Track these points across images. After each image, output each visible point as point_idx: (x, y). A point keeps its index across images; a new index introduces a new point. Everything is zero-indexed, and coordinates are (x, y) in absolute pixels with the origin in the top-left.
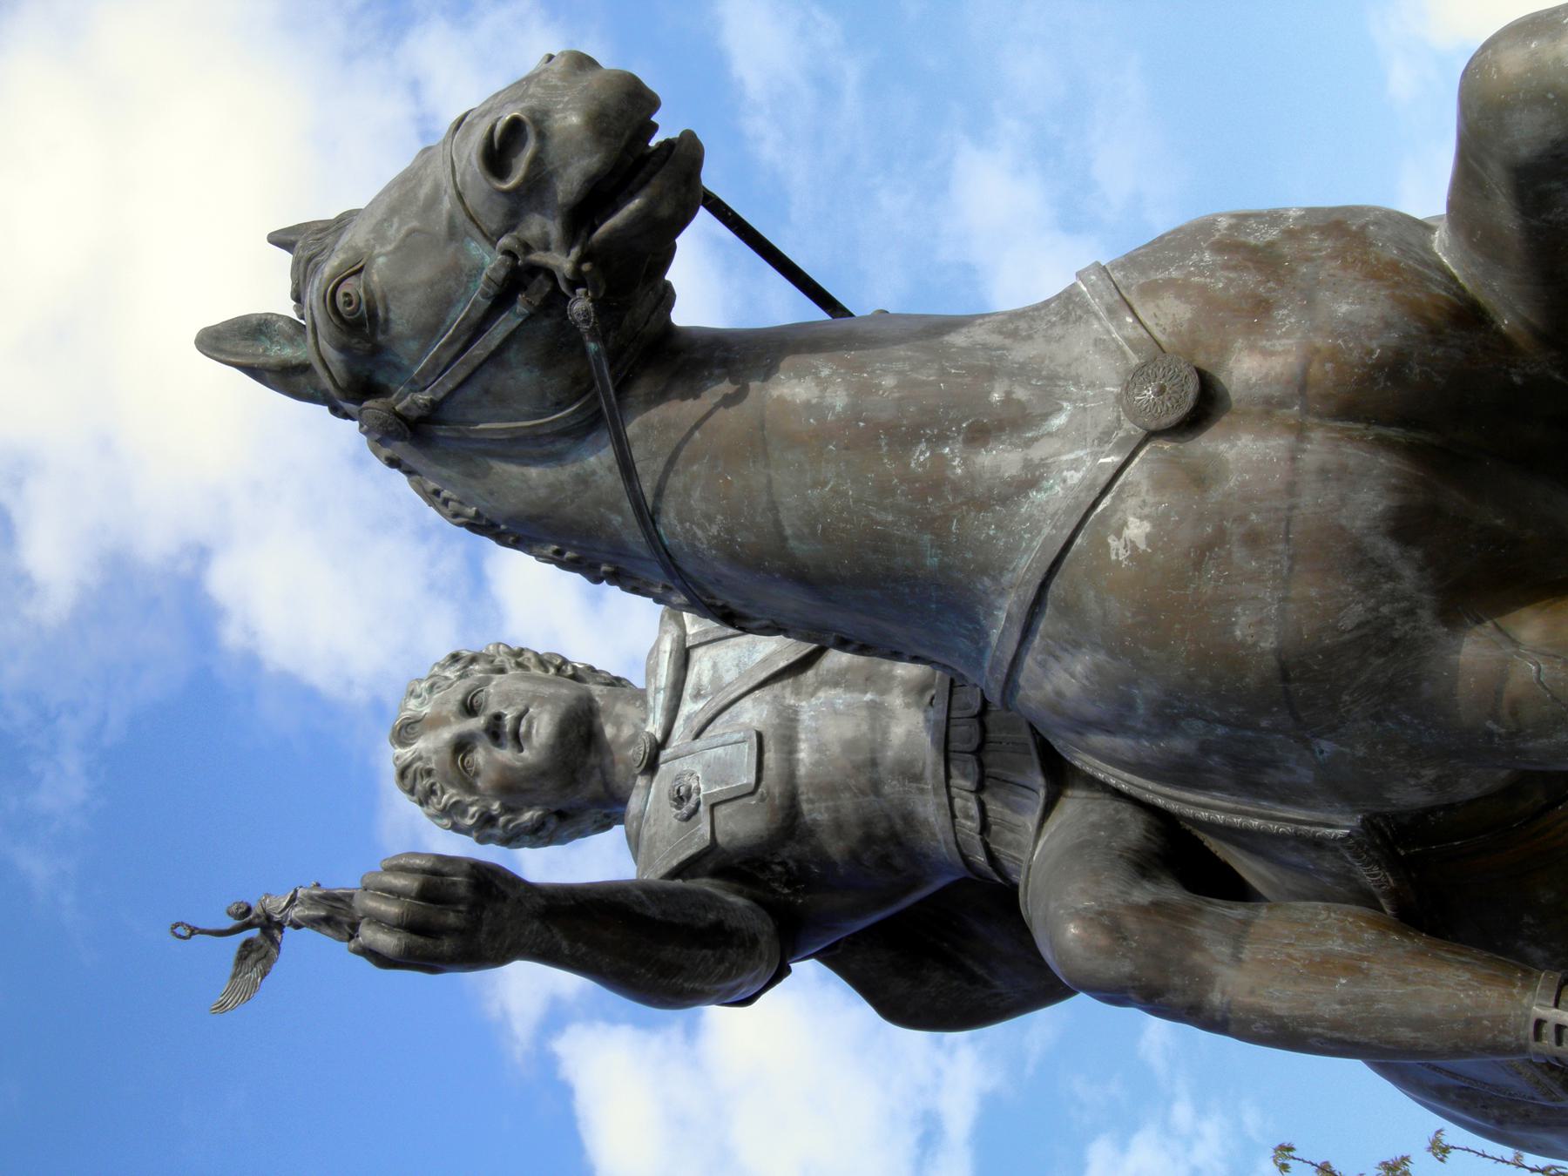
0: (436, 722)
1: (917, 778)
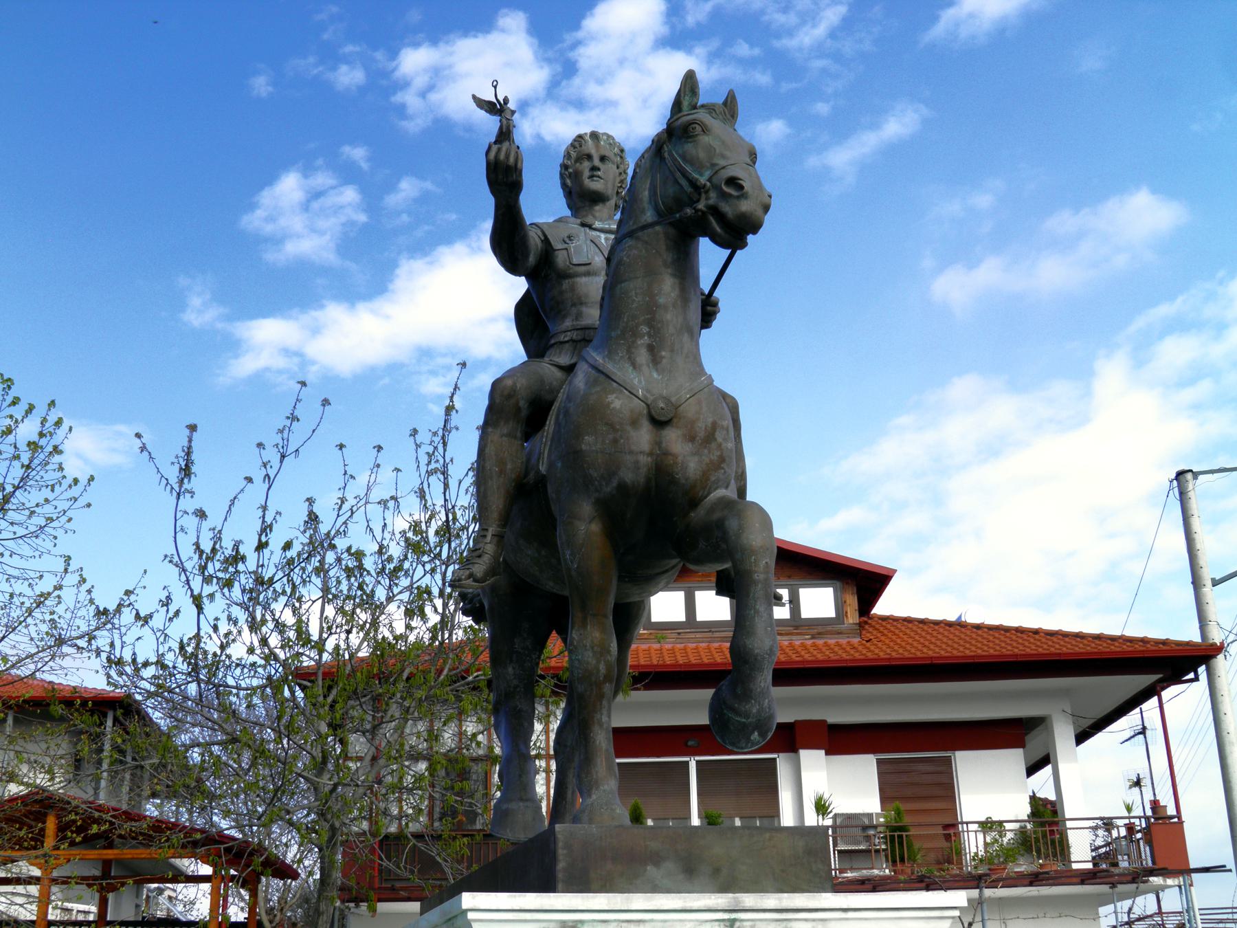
0: (597, 146)
1: (577, 319)
